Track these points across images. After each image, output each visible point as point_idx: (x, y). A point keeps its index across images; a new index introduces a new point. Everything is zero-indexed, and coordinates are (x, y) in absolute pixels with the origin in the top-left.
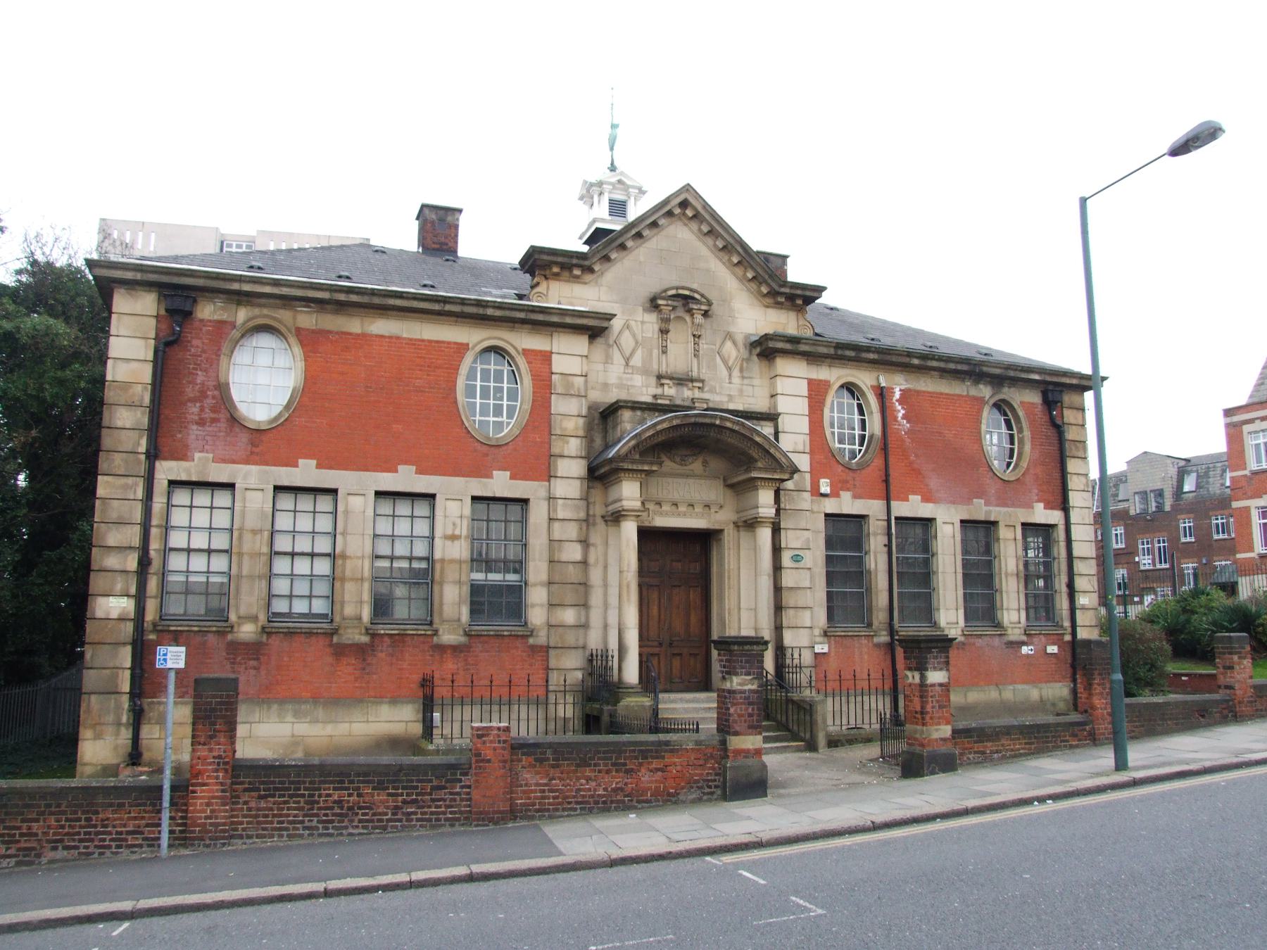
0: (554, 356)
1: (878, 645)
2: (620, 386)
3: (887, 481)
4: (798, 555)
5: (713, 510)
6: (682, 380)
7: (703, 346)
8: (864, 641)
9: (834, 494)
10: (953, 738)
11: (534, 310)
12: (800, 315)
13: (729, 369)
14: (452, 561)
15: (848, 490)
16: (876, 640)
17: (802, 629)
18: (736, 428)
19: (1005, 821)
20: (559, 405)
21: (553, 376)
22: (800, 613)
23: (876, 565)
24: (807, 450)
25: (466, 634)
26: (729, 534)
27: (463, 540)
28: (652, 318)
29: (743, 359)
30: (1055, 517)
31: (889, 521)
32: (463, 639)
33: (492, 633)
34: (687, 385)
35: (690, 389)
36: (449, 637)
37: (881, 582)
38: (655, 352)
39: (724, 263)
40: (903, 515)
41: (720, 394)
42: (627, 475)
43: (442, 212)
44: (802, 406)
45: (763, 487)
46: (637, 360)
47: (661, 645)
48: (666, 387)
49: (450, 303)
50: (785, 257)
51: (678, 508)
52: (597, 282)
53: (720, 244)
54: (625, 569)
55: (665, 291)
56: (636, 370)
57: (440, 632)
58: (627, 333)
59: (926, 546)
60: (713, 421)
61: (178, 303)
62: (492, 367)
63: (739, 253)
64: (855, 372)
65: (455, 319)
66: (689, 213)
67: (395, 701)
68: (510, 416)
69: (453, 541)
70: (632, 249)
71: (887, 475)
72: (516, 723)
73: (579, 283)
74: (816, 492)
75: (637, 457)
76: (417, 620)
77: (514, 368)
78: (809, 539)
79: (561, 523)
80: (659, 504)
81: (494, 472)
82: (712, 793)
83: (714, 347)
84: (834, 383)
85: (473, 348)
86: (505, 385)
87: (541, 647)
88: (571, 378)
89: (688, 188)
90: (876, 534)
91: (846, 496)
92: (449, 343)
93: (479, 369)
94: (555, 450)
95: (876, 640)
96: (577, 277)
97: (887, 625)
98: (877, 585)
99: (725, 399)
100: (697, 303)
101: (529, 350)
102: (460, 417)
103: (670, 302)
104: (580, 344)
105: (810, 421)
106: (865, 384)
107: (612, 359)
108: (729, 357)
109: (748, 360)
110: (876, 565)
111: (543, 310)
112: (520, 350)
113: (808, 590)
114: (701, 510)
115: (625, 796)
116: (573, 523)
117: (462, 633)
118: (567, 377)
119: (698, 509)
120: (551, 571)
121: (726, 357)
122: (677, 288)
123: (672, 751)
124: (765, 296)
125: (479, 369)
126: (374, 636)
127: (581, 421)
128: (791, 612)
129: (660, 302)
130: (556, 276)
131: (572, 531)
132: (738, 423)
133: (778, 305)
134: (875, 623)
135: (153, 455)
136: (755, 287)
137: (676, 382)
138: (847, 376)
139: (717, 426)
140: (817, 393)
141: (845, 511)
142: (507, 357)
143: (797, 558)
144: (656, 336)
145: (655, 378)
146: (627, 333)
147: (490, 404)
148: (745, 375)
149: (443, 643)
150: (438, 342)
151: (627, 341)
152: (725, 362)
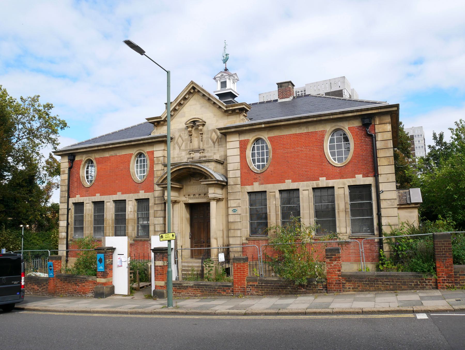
13: (214, 143)
15: (257, 182)
30: (369, 180)
42: (214, 185)
44: (237, 152)
46: (183, 147)
61: (367, 121)
78: (239, 203)
84: (250, 140)
88: (159, 158)
89: (192, 82)
101: (148, 152)
104: (162, 147)
105: (240, 157)
108: (214, 138)
111: (352, 111)
119: (192, 196)
135: (69, 197)
140: (243, 147)
141: (255, 190)
143: (234, 211)
151: (180, 141)
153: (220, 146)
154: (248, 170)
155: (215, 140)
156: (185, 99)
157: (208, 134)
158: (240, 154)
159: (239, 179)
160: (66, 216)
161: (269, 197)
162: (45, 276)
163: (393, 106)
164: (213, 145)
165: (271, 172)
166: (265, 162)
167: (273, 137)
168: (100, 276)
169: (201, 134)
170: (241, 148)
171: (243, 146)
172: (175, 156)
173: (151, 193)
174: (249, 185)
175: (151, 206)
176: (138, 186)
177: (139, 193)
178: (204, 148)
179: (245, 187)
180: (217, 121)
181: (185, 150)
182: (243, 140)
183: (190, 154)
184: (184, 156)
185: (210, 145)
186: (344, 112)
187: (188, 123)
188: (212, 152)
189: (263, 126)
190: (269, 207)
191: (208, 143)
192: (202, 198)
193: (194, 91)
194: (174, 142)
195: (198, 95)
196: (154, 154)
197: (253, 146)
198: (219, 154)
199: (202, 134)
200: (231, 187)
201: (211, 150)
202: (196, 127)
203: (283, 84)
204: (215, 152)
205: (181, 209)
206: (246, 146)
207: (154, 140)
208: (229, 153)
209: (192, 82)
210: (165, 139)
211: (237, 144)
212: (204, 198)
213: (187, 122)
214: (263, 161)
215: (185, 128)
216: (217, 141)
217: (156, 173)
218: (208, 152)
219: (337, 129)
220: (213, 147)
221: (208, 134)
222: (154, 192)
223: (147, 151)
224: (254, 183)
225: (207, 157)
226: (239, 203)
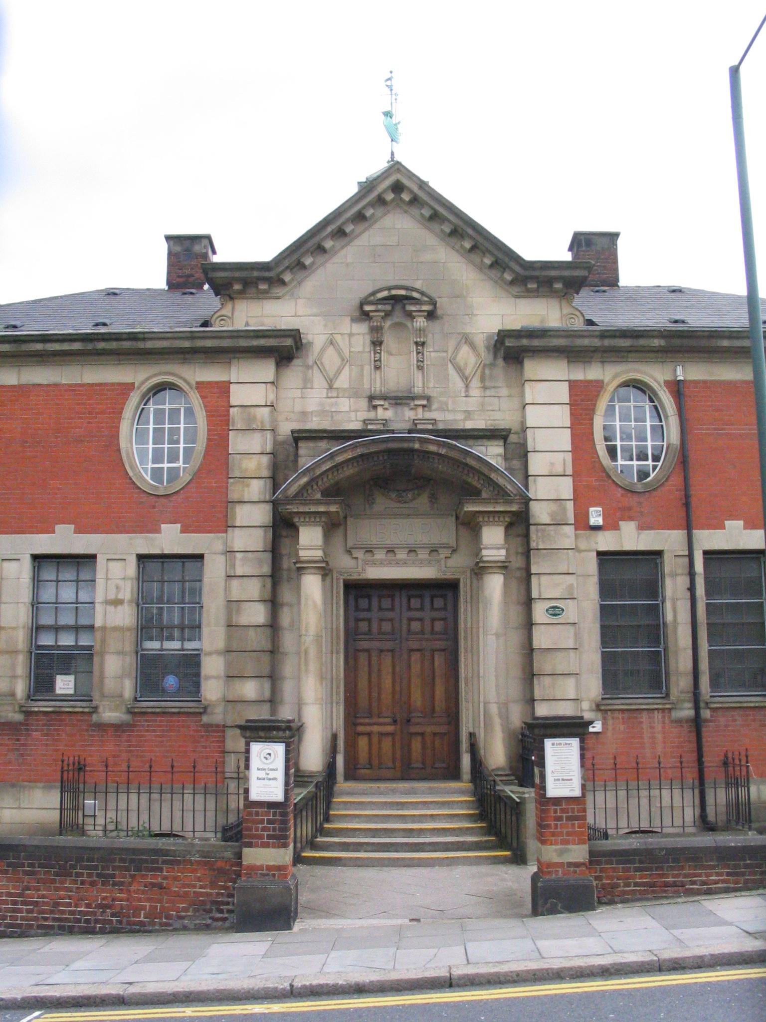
0: (233, 388)
1: (679, 721)
2: (323, 413)
3: (687, 505)
4: (558, 608)
5: (442, 556)
6: (399, 400)
7: (430, 354)
8: (657, 716)
9: (611, 524)
10: (591, 862)
11: (218, 335)
12: (564, 303)
13: (466, 380)
14: (115, 629)
15: (631, 519)
16: (676, 714)
17: (561, 703)
18: (443, 451)
19: (588, 995)
20: (238, 443)
21: (231, 410)
22: (560, 681)
23: (675, 616)
24: (569, 471)
25: (129, 711)
27: (126, 605)
28: (362, 328)
29: (485, 366)
31: (691, 556)
32: (126, 718)
33: (158, 710)
34: (408, 404)
35: (412, 409)
36: (110, 714)
37: (682, 637)
38: (367, 369)
39: (457, 251)
40: (716, 547)
41: (454, 411)
43: (188, 242)
44: (562, 416)
45: (488, 523)
46: (343, 381)
47: (395, 721)
48: (380, 410)
49: (98, 340)
50: (614, 236)
51: (417, 555)
52: (292, 295)
53: (447, 229)
54: (304, 633)
55: (374, 293)
56: (341, 393)
57: (101, 709)
58: (331, 351)
59: (654, 588)
60: (411, 445)
62: (167, 407)
63: (471, 237)
64: (170, 367)
65: (182, 356)
66: (406, 197)
67: (48, 788)
68: (656, 458)
69: (116, 607)
70: (334, 252)
71: (687, 497)
72: (125, 813)
73: (270, 298)
74: (582, 523)
75: (318, 496)
76: (85, 696)
77: (657, 403)
79: (240, 580)
80: (369, 551)
81: (163, 526)
82: (224, 920)
83: (444, 354)
84: (608, 384)
85: (139, 388)
86: (618, 423)
87: (218, 726)
88: (252, 410)
90: (674, 575)
91: (628, 528)
92: (112, 384)
93: (152, 409)
94: (234, 495)
95: (676, 714)
96: (266, 292)
97: (691, 695)
98: (676, 639)
99: (460, 416)
100: (416, 304)
101: (203, 383)
102: (124, 465)
103: (380, 307)
104: (266, 370)
105: (572, 435)
106: (655, 380)
107: (312, 382)
108: (466, 364)
109: (492, 365)
110: (675, 616)
112: (194, 385)
113: (572, 653)
114: (426, 556)
115: (113, 915)
116: (255, 580)
117: (124, 709)
118: (247, 409)
119: (423, 555)
120: (229, 638)
122: (389, 289)
123: (172, 863)
124: (512, 283)
125: (152, 409)
126: (28, 713)
127: (265, 460)
128: (547, 680)
129: (367, 308)
130: (242, 294)
131: (254, 589)
132: (444, 445)
133: (529, 294)
134: (675, 692)
136: (499, 275)
137: (393, 402)
138: (625, 372)
139: (417, 450)
142: (648, 392)
143: (555, 611)
144: (367, 349)
145: (366, 400)
146: (331, 351)
147: (168, 448)
148: (487, 384)
149: (105, 722)
150: (100, 385)
151: (331, 359)
152: (460, 370)
158: (571, 424)
159: (570, 506)
168: (261, 837)
169: (416, 343)
170: (573, 404)
176: (154, 507)
177: (158, 531)
178: (428, 392)
183: (375, 407)
192: (421, 563)
196: (229, 392)
197: (143, 409)
199: (423, 344)
205: (335, 601)
206: (591, 400)
208: (534, 416)
210: (746, 343)
211: (563, 393)
212: (430, 563)
216: (479, 373)
219: (645, 382)
222: (226, 532)
223: (198, 380)
224: (621, 523)
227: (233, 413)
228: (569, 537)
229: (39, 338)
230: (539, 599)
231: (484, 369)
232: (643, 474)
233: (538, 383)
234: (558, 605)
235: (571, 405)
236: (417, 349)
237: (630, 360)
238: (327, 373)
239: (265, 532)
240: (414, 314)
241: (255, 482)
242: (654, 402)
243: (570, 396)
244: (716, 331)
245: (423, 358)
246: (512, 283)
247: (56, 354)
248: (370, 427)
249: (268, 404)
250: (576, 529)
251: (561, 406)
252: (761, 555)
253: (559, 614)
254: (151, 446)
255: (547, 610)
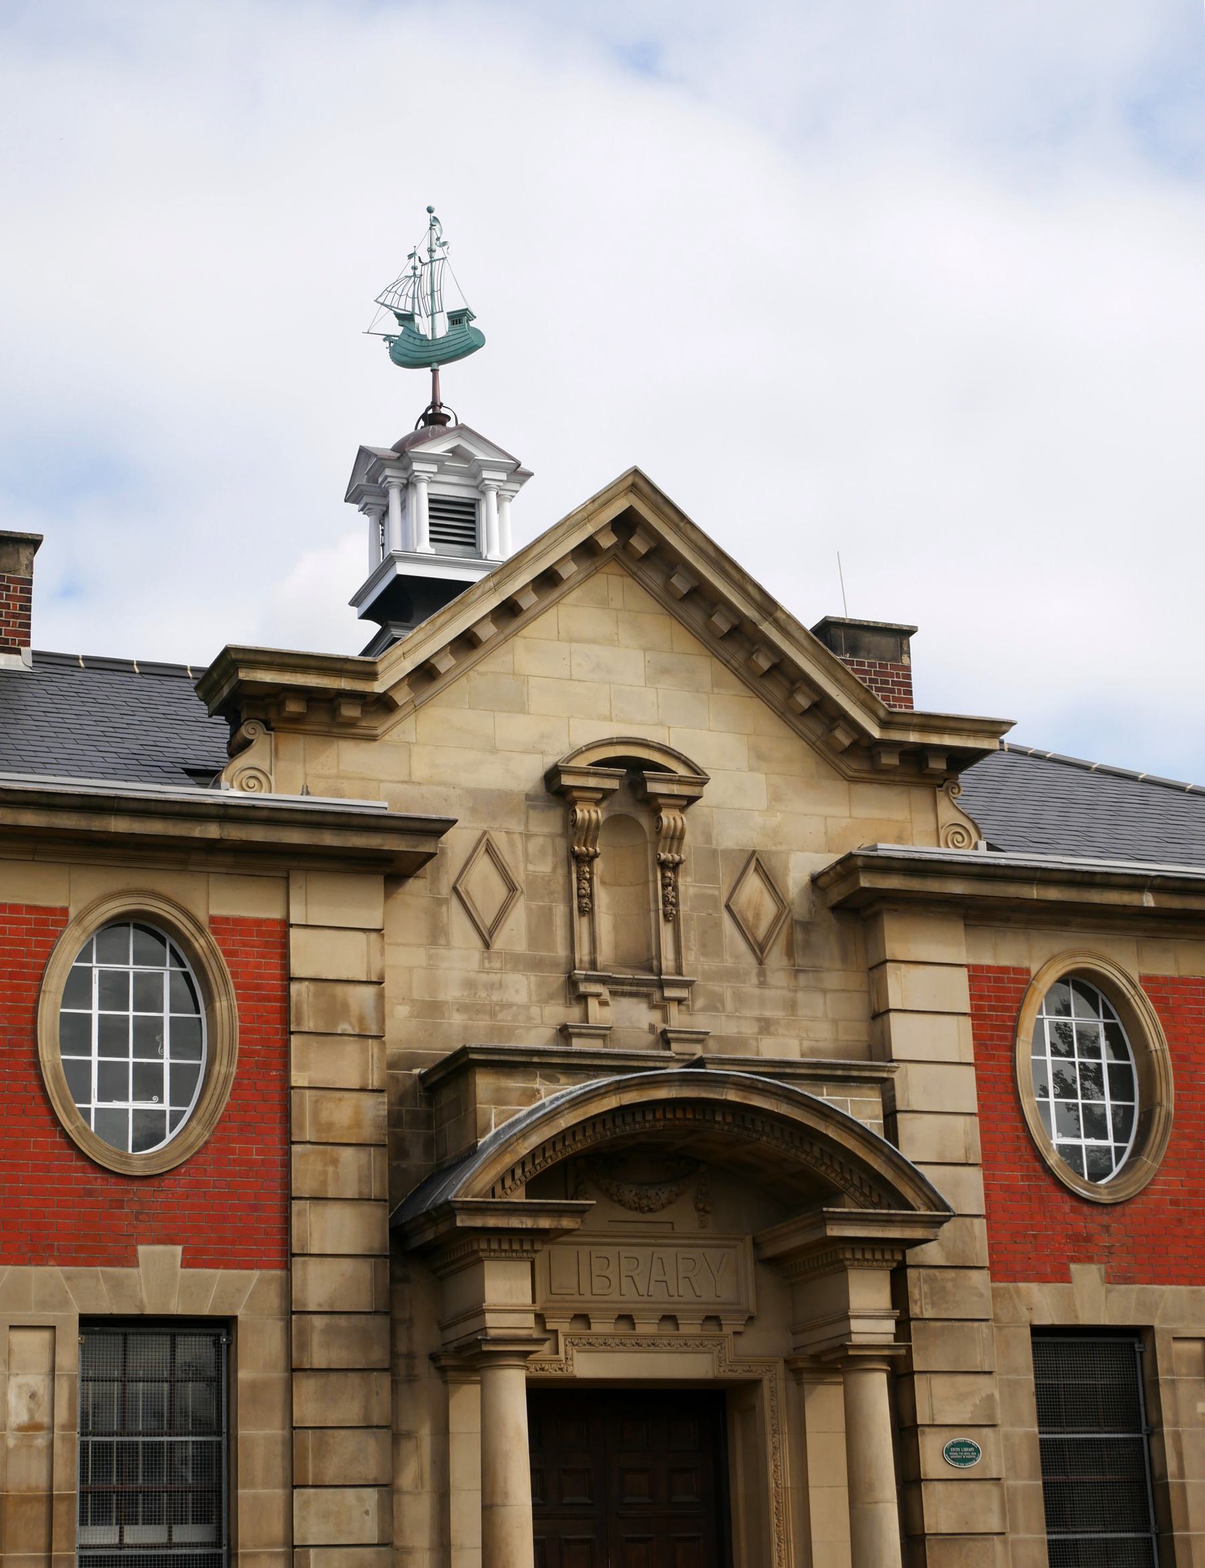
4: (970, 1446)
5: (728, 1330)
13: (759, 949)
15: (1090, 1260)
21: (294, 987)
26: (774, 1393)
45: (864, 1264)
51: (677, 1325)
66: (639, 545)
81: (141, 1249)
85: (80, 919)
88: (339, 990)
89: (636, 482)
101: (226, 920)
105: (978, 1078)
108: (757, 916)
119: (689, 1328)
121: (750, 915)
124: (848, 752)
125: (95, 972)
138: (1073, 954)
143: (960, 1453)
153: (802, 977)
154: (1028, 1178)
155: (761, 932)
156: (548, 580)
157: (713, 878)
160: (931, 1423)
161: (1170, 1371)
162: (651, 1193)
163: (1193, 885)
164: (749, 960)
165: (1175, 1203)
166: (101, 1098)
167: (1173, 980)
169: (663, 865)
171: (992, 1008)
172: (442, 997)
173: (256, 1274)
174: (1043, 1279)
175: (253, 1385)
176: (120, 1204)
177: (130, 1260)
179: (1018, 1291)
180: (776, 797)
181: (535, 964)
182: (989, 968)
184: (527, 1007)
185: (729, 962)
186: (232, 811)
187: (582, 762)
188: (747, 1013)
189: (1149, 900)
190: (1177, 1437)
191: (711, 944)
192: (687, 1346)
193: (624, 545)
194: (435, 880)
195: (630, 581)
198: (801, 1040)
199: (675, 866)
200: (931, 1280)
201: (739, 998)
202: (624, 810)
203: (868, 639)
204: (768, 1014)
207: (329, 839)
209: (636, 482)
213: (579, 752)
214: (148, 1083)
215: (528, 797)
217: (316, 1112)
218: (715, 1005)
220: (755, 980)
221: (713, 878)
223: (214, 912)
224: (1073, 1267)
225: (711, 1043)
226: (991, 1397)
227: (299, 994)
228: (981, 1295)
229: (77, 801)
230: (929, 1426)
231: (791, 927)
232: (150, 1132)
233: (911, 966)
234: (969, 1440)
235: (976, 1015)
236: (663, 877)
237: (191, 868)
238: (753, 935)
239: (375, 1269)
240: (661, 801)
241: (347, 1154)
242: (184, 966)
243: (972, 997)
244: (254, 807)
245: (677, 897)
246: (848, 752)
247: (211, 847)
248: (578, 1045)
249: (374, 979)
250: (994, 1278)
251: (955, 1018)
252: (1135, 1340)
253: (971, 1460)
254: (95, 1058)
255: (948, 1451)
